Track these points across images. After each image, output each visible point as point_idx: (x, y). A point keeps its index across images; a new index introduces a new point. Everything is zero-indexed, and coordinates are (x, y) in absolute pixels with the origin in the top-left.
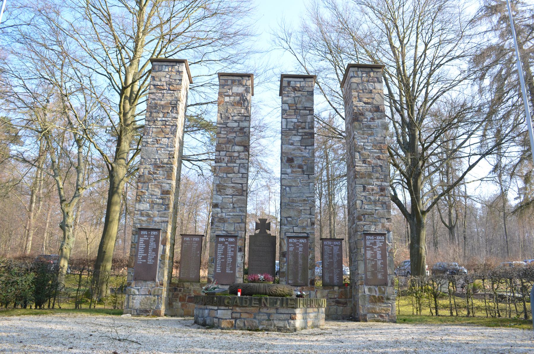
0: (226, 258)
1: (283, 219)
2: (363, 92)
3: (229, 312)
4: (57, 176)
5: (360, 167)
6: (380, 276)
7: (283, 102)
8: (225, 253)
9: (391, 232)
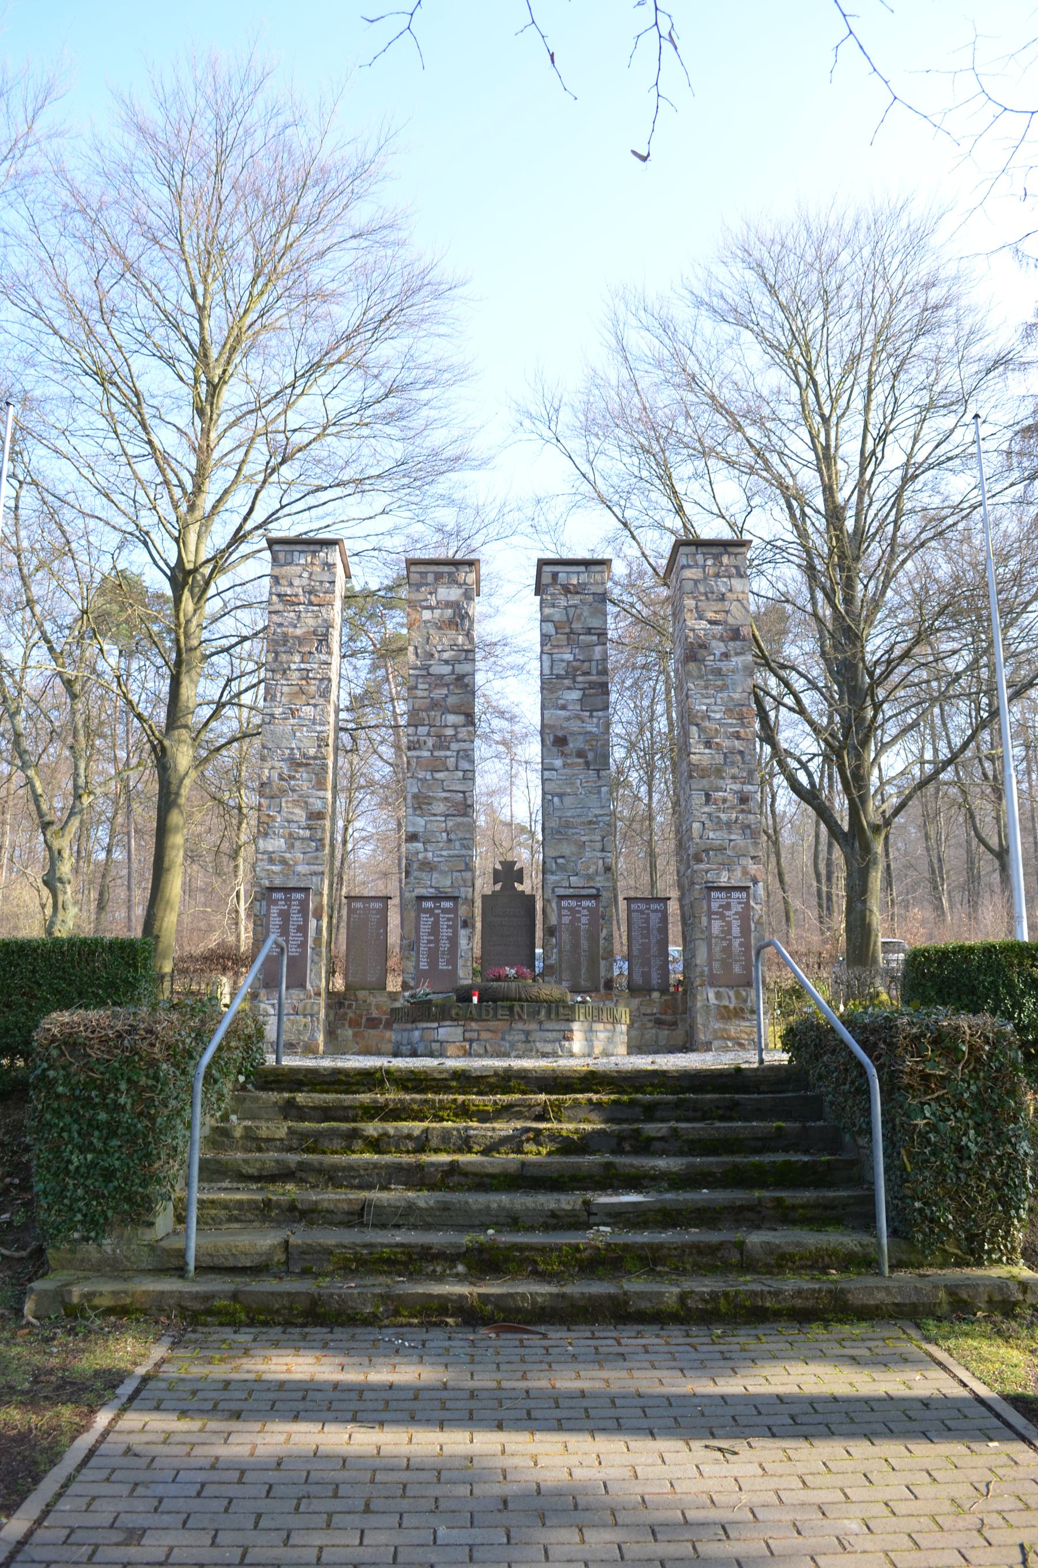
0: (437, 941)
1: (548, 860)
2: (707, 598)
3: (460, 1030)
4: (29, 767)
5: (700, 754)
6: (737, 969)
7: (544, 620)
8: (435, 930)
9: (761, 884)
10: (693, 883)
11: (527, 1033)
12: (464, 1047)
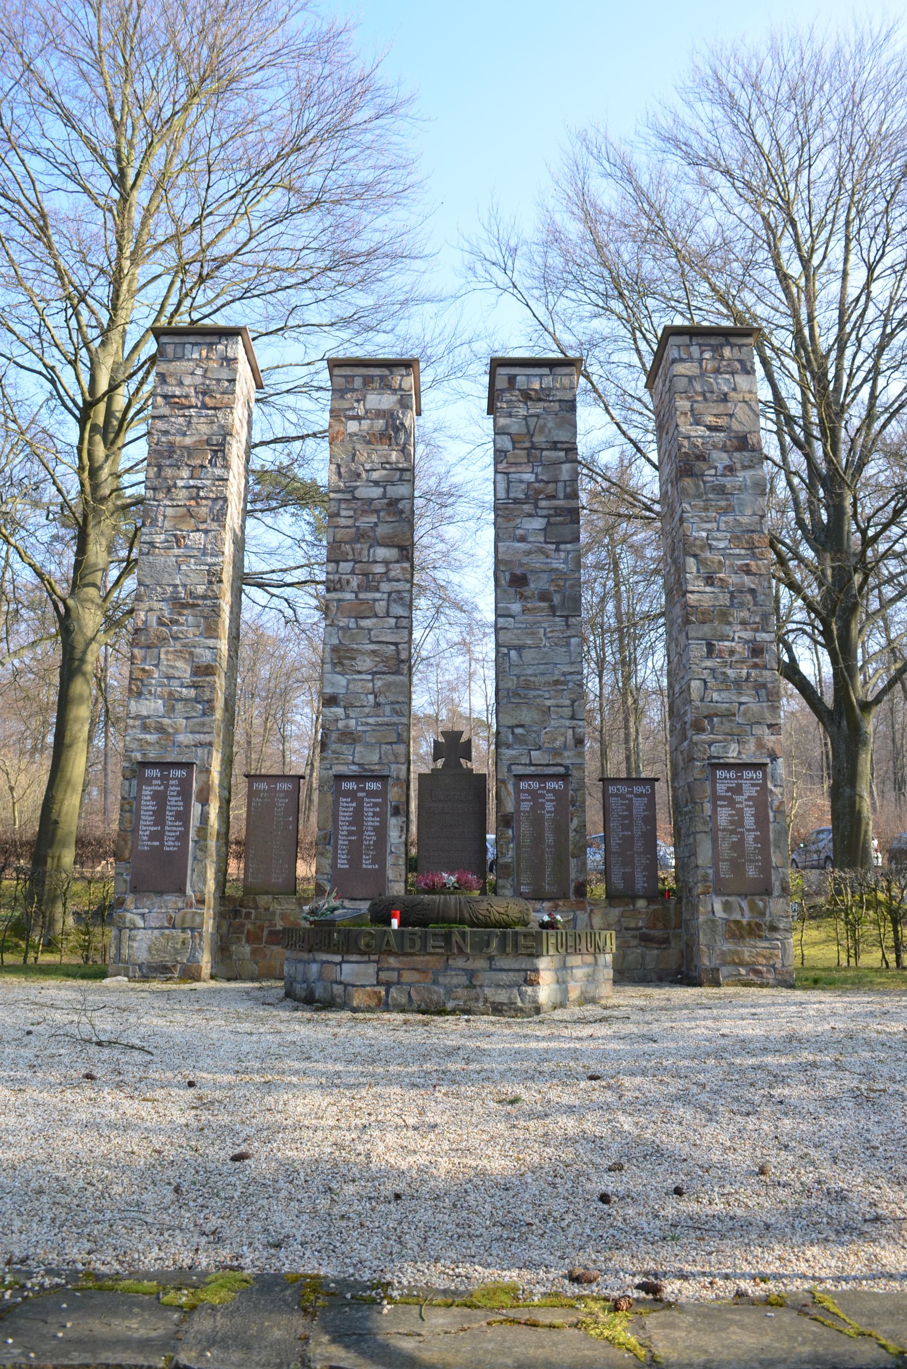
0: (360, 832)
1: (502, 730)
2: (705, 399)
3: (372, 969)
6: (751, 872)
7: (499, 431)
8: (358, 818)
10: (692, 759)
11: (471, 974)
12: (377, 994)
